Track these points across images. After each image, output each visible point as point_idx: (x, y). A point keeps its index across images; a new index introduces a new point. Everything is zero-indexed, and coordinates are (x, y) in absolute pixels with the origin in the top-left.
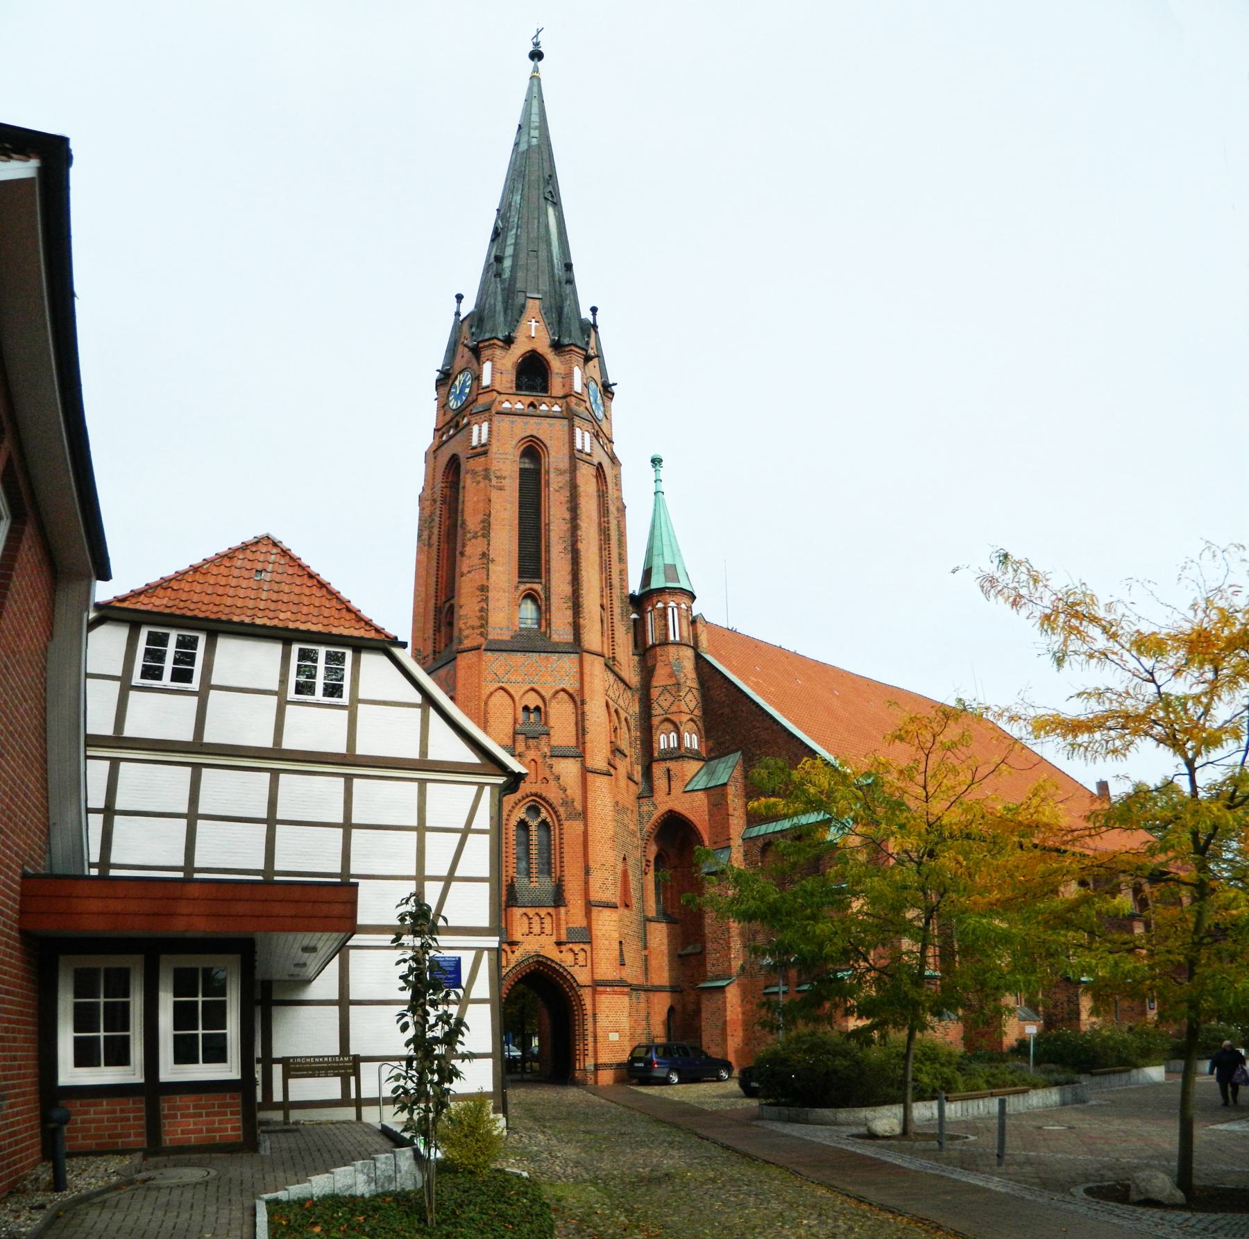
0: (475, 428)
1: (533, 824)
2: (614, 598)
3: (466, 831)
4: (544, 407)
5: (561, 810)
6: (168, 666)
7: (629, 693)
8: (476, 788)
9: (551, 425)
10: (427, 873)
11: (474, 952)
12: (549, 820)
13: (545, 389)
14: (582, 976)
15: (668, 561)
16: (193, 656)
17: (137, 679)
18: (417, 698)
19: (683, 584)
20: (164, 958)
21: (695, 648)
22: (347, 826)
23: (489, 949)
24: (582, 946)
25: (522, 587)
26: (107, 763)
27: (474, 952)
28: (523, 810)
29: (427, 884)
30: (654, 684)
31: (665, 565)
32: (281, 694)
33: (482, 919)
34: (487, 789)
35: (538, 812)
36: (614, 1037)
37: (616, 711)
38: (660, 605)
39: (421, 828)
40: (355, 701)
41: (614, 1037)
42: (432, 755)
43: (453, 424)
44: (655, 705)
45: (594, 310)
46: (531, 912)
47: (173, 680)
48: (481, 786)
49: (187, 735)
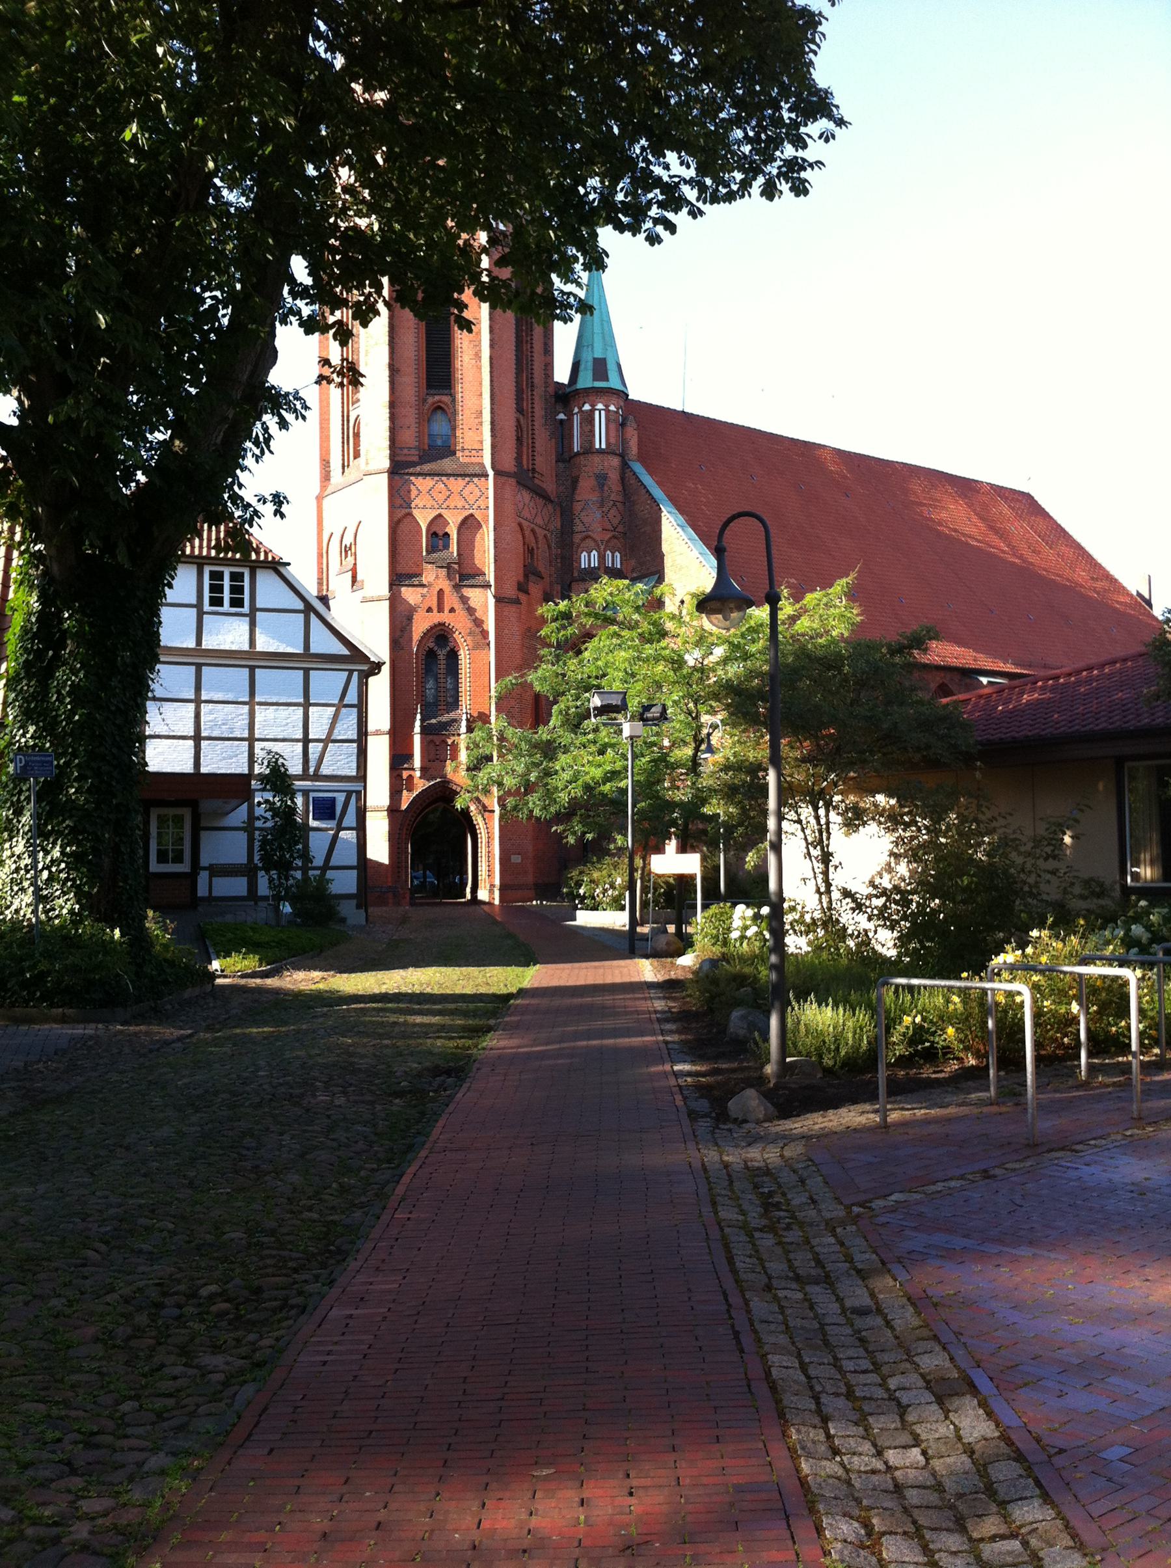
2: (536, 398)
7: (550, 507)
10: (311, 737)
15: (598, 354)
17: (207, 607)
18: (300, 605)
19: (614, 383)
20: (152, 809)
21: (622, 456)
22: (251, 703)
25: (431, 400)
30: (577, 498)
31: (595, 360)
32: (199, 606)
34: (356, 673)
37: (533, 531)
38: (587, 407)
40: (254, 609)
42: (314, 649)
44: (577, 521)
48: (351, 672)
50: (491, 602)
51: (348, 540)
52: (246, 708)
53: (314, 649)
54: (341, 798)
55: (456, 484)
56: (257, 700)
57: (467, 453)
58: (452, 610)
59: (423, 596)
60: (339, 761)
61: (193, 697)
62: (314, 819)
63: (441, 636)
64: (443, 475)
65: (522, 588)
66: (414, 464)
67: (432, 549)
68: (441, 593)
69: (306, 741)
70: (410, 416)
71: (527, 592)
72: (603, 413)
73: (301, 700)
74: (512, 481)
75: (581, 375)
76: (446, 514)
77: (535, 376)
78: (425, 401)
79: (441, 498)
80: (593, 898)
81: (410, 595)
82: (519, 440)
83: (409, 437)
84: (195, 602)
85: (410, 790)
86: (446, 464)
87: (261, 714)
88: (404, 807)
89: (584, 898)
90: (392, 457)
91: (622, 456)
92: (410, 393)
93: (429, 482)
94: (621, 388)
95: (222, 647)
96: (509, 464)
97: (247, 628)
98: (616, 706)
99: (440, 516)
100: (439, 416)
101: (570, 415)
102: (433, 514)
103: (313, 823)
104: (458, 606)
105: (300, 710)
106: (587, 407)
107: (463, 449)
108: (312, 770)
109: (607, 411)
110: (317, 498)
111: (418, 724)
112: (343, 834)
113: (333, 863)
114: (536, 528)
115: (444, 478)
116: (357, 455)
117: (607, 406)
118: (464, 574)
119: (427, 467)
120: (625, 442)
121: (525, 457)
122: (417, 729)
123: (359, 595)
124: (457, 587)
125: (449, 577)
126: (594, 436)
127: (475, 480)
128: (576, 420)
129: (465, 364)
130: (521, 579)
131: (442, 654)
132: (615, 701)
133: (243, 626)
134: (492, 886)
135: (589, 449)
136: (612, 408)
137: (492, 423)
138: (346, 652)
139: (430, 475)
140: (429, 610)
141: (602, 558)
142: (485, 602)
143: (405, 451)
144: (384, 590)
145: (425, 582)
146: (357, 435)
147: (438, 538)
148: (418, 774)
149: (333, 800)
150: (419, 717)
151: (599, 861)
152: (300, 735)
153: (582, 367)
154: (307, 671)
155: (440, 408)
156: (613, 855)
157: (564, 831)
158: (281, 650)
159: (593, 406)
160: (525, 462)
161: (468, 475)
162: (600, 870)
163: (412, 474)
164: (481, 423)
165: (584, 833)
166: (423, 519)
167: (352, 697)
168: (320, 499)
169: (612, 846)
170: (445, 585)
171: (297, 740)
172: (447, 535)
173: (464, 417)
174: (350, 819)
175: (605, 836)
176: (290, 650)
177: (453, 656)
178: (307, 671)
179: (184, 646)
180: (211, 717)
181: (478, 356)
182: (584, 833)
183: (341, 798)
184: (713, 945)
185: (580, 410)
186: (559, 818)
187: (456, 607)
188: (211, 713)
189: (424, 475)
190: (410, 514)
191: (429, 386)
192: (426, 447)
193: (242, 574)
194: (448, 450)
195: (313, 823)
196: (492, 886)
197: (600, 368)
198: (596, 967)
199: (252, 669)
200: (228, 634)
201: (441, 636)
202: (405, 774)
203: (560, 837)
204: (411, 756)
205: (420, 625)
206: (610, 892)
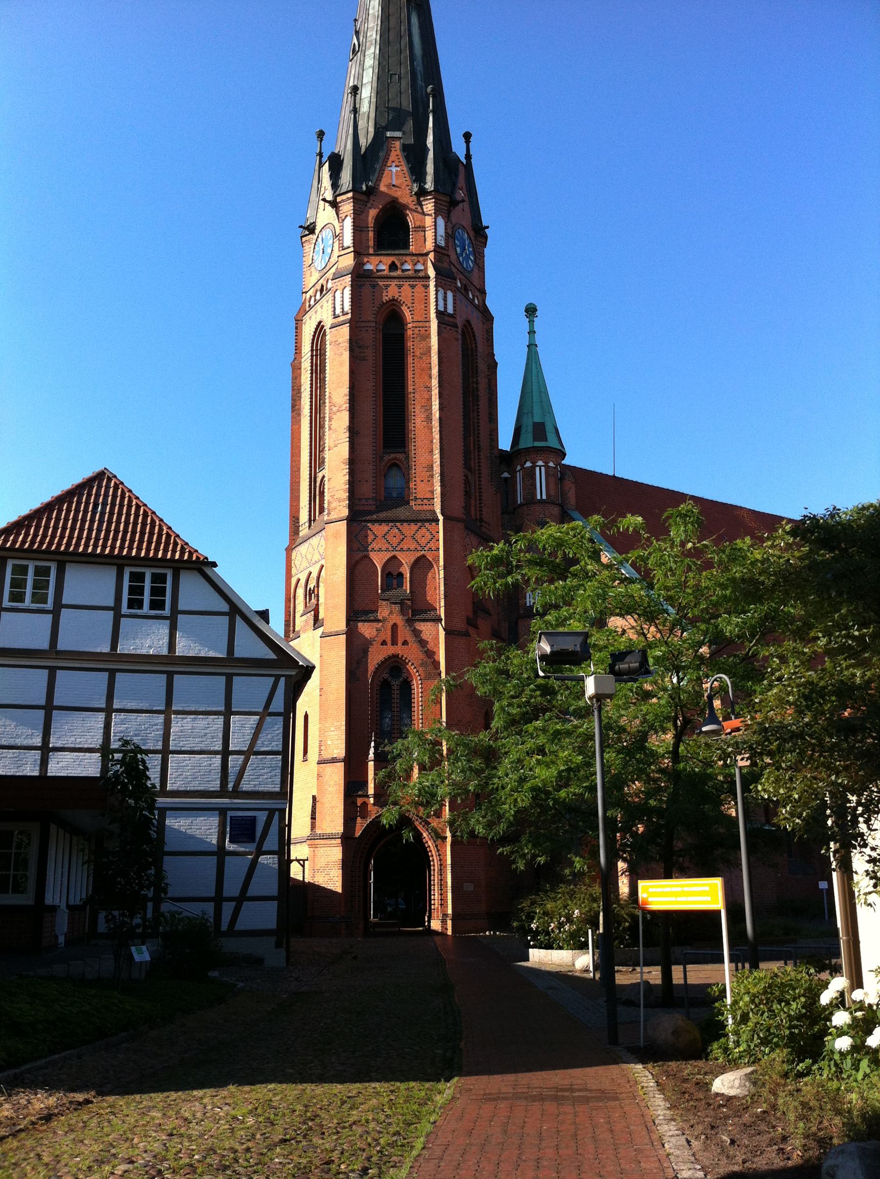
6: (147, 597)
8: (273, 679)
13: (406, 245)
15: (537, 419)
16: (152, 594)
17: (125, 610)
18: (225, 607)
19: (552, 442)
25: (387, 458)
26: (46, 672)
28: (387, 670)
31: (535, 424)
32: (116, 609)
34: (283, 679)
38: (528, 464)
40: (59, 606)
42: (239, 653)
45: (467, 136)
47: (32, 602)
48: (277, 678)
49: (45, 645)
50: (442, 634)
51: (312, 585)
52: (161, 718)
53: (239, 653)
54: (262, 817)
55: (409, 529)
56: (174, 708)
57: (419, 502)
58: (405, 643)
59: (378, 630)
61: (104, 706)
62: (230, 841)
63: (395, 667)
64: (397, 521)
65: (471, 622)
66: (371, 513)
67: (386, 587)
68: (395, 627)
69: (225, 753)
70: (367, 472)
71: (476, 627)
72: (543, 469)
73: (222, 708)
74: (461, 526)
75: (523, 436)
76: (401, 556)
77: (481, 432)
78: (382, 458)
79: (395, 541)
80: (548, 933)
81: (366, 630)
82: (467, 493)
83: (366, 490)
84: (112, 604)
85: (364, 817)
86: (401, 512)
87: (178, 725)
88: (358, 834)
89: (536, 933)
90: (351, 507)
91: (562, 506)
92: (367, 451)
93: (384, 528)
94: (558, 447)
95: (139, 652)
96: (458, 509)
97: (167, 631)
98: (574, 653)
99: (394, 557)
100: (394, 472)
101: (513, 473)
102: (389, 555)
103: (230, 846)
104: (411, 639)
105: (220, 720)
106: (528, 464)
107: (416, 499)
108: (230, 786)
110: (286, 549)
111: (372, 751)
112: (263, 859)
113: (251, 892)
116: (322, 510)
117: (546, 463)
118: (417, 609)
119: (383, 515)
120: (563, 494)
121: (473, 508)
122: (371, 755)
123: (320, 631)
124: (410, 622)
125: (403, 612)
127: (427, 525)
129: (417, 425)
130: (471, 616)
131: (395, 684)
132: (572, 645)
133: (162, 630)
134: (445, 915)
135: (530, 499)
136: (551, 464)
137: (442, 475)
138: (272, 656)
139: (385, 521)
140: (384, 643)
142: (438, 636)
143: (364, 502)
144: (342, 626)
145: (380, 618)
146: (322, 494)
147: (392, 577)
148: (372, 800)
149: (253, 819)
150: (373, 744)
151: (552, 890)
152: (218, 747)
153: (523, 431)
154: (229, 678)
155: (395, 465)
156: (569, 883)
157: (512, 852)
158: (202, 654)
159: (534, 463)
160: (473, 512)
161: (421, 521)
162: (554, 900)
163: (369, 521)
164: (432, 476)
165: (534, 856)
166: (378, 560)
167: (278, 704)
168: (289, 550)
169: (567, 871)
170: (399, 619)
171: (216, 753)
172: (401, 575)
173: (418, 471)
174: (271, 842)
175: (558, 859)
176: (212, 654)
177: (407, 686)
178: (229, 678)
179: (98, 651)
180: (123, 727)
181: (429, 419)
182: (534, 856)
184: (418, 804)
186: (505, 840)
187: (409, 639)
188: (123, 722)
189: (380, 521)
190: (367, 557)
191: (386, 446)
192: (383, 499)
193: (164, 576)
194: (403, 499)
195: (230, 846)
196: (445, 915)
197: (540, 430)
198: (558, 1096)
199: (170, 675)
200: (148, 639)
201: (395, 667)
202: (359, 801)
203: (506, 861)
204: (366, 783)
205: (375, 657)
206: (567, 927)
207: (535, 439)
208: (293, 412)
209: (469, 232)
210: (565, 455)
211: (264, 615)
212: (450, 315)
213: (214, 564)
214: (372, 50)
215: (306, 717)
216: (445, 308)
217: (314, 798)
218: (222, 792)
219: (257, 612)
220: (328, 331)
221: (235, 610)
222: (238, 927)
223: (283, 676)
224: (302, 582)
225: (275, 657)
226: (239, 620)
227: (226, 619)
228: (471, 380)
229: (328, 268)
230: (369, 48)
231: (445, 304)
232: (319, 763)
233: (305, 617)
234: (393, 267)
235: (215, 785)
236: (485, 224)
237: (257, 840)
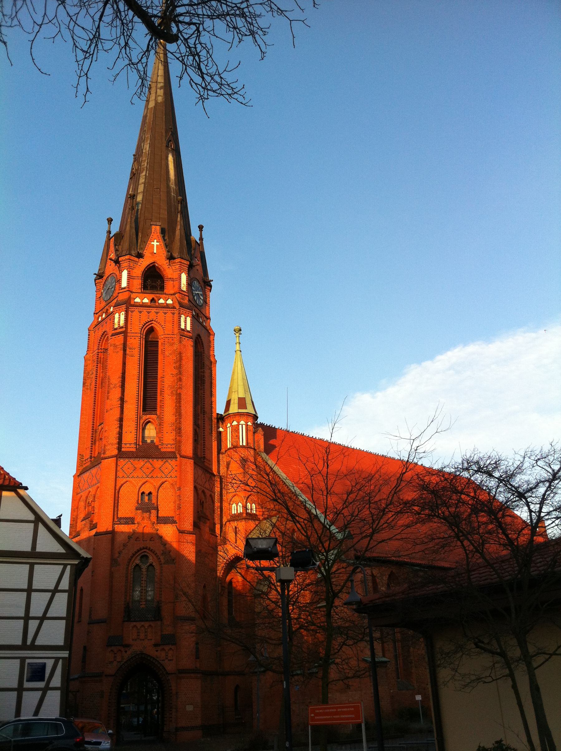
0: (117, 316)
1: (144, 567)
3: (55, 591)
4: (161, 301)
5: (162, 558)
8: (62, 567)
9: (165, 313)
11: (54, 660)
12: (154, 564)
13: (162, 288)
14: (170, 667)
15: (241, 395)
18: (32, 517)
23: (63, 658)
24: (170, 646)
25: (144, 417)
27: (54, 660)
28: (139, 558)
29: (31, 622)
33: (60, 641)
34: (69, 567)
35: (146, 557)
36: (190, 708)
37: (203, 491)
38: (235, 423)
39: (30, 590)
41: (190, 708)
42: (39, 549)
43: (105, 310)
45: (201, 228)
46: (139, 624)
48: (65, 566)
54: (50, 664)
60: (330, 703)
106: (235, 423)
108: (29, 642)
109: (247, 425)
113: (48, 615)
114: (206, 490)
115: (151, 460)
121: (199, 450)
126: (239, 438)
128: (229, 430)
138: (62, 550)
141: (245, 507)
143: (128, 445)
153: (232, 402)
154: (32, 566)
159: (238, 422)
178: (32, 566)
183: (50, 664)
185: (231, 426)
191: (144, 410)
207: (239, 408)
208: (83, 387)
209: (202, 282)
210: (257, 417)
211: (58, 521)
212: (188, 332)
213: (26, 488)
214: (144, 174)
215: (82, 590)
216: (185, 327)
217: (85, 648)
218: (24, 646)
219: (53, 520)
220: (110, 337)
221: (38, 519)
222: (38, 643)
223: (60, 658)
224: (84, 498)
225: (64, 552)
226: (41, 527)
227: (32, 525)
228: (200, 371)
229: (111, 299)
230: (142, 172)
231: (186, 325)
232: (89, 624)
233: (84, 522)
234: (153, 300)
235: (19, 642)
236: (210, 278)
237: (46, 679)
